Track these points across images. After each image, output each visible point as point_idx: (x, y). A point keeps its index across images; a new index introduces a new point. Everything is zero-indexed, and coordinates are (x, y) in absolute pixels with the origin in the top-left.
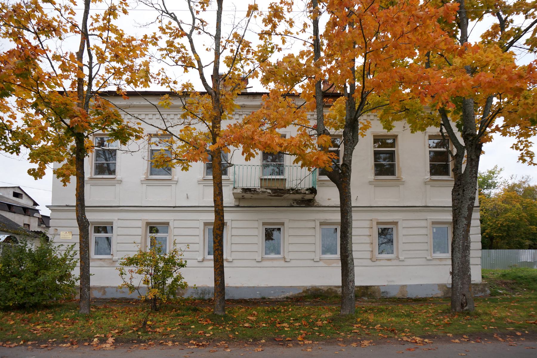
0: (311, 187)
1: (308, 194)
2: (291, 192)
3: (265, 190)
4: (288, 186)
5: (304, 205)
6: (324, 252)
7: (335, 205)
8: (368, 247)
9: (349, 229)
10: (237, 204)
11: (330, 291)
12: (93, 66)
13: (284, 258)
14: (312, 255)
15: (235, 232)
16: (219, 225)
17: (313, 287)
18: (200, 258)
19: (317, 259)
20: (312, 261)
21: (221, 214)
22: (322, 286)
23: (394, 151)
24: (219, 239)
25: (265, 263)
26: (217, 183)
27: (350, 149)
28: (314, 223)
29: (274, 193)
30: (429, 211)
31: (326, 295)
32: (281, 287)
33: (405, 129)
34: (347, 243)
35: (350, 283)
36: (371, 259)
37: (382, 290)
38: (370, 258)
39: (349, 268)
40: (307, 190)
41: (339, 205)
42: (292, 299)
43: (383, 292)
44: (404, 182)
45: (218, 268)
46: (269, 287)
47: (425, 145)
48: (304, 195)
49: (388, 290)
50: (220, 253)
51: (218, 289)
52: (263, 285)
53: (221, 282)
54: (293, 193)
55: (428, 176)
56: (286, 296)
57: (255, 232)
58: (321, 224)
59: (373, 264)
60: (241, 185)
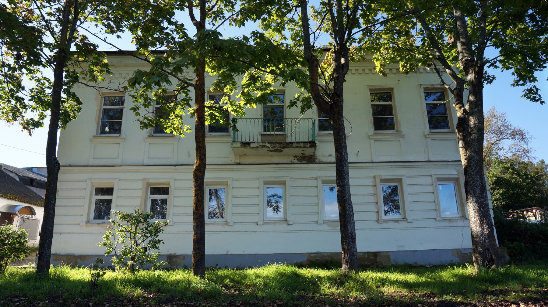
0: (310, 140)
5: (305, 162)
8: (373, 208)
12: (118, 50)
30: (432, 166)
36: (377, 221)
38: (376, 219)
41: (335, 162)
44: (404, 135)
47: (421, 98)
48: (304, 149)
55: (427, 129)
59: (380, 226)
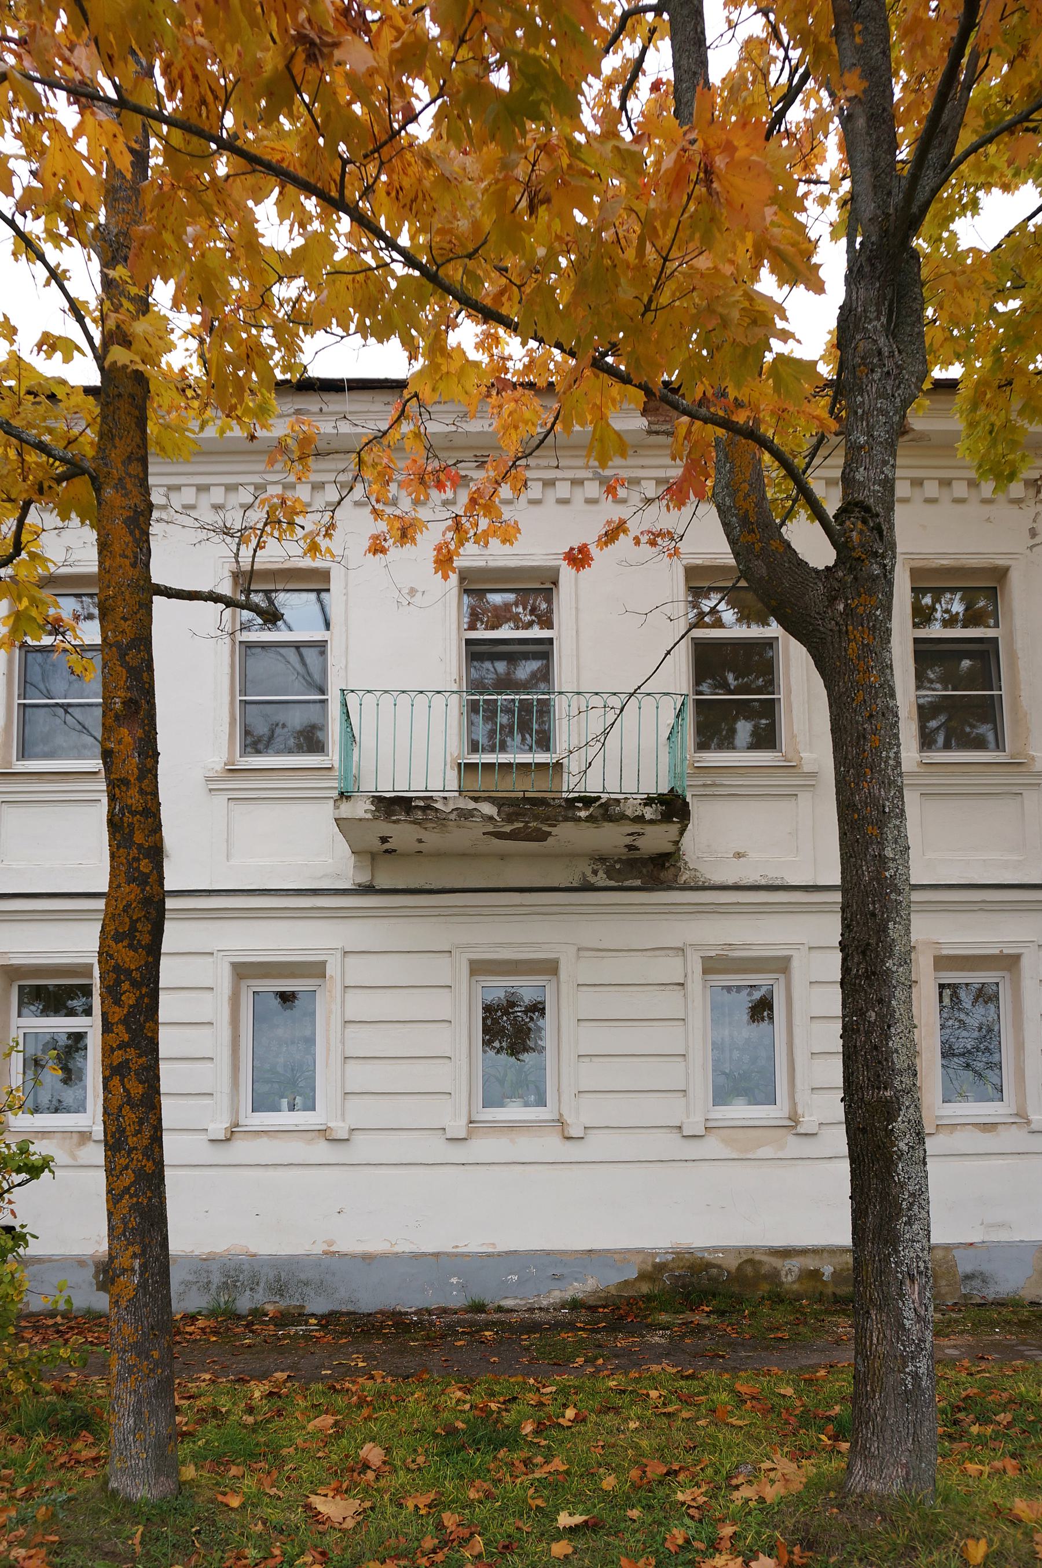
0: (664, 789)
1: (652, 822)
2: (583, 814)
3: (472, 805)
4: (570, 785)
5: (638, 883)
6: (721, 1097)
7: (763, 882)
9: (894, 931)
10: (364, 878)
11: (749, 1270)
13: (561, 1122)
14: (671, 1111)
15: (359, 1005)
16: (127, 908)
17: (679, 1254)
18: (218, 1127)
19: (694, 1125)
20: (675, 1136)
21: (138, 838)
22: (715, 1250)
23: (995, 641)
24: (129, 999)
25: (483, 1147)
26: (118, 645)
27: (882, 411)
28: (678, 961)
29: (509, 819)
31: (736, 1289)
32: (548, 1253)
33: (1037, 540)
34: (886, 1022)
35: (907, 1287)
37: (965, 1267)
39: (902, 1185)
40: (649, 801)
42: (592, 1309)
43: (968, 1277)
45: (127, 1190)
46: (499, 1254)
49: (986, 1268)
50: (137, 1090)
51: (128, 1330)
52: (475, 1243)
53: (143, 1285)
54: (590, 819)
56: (568, 1295)
57: (441, 1005)
58: (712, 966)
60: (368, 785)
